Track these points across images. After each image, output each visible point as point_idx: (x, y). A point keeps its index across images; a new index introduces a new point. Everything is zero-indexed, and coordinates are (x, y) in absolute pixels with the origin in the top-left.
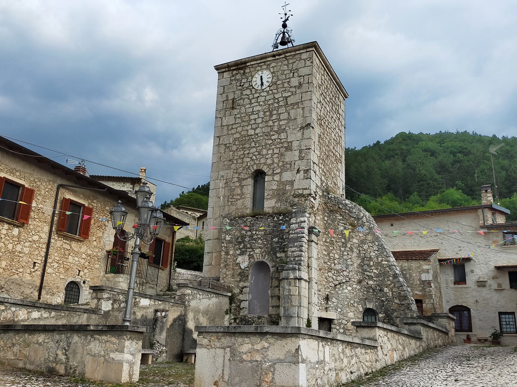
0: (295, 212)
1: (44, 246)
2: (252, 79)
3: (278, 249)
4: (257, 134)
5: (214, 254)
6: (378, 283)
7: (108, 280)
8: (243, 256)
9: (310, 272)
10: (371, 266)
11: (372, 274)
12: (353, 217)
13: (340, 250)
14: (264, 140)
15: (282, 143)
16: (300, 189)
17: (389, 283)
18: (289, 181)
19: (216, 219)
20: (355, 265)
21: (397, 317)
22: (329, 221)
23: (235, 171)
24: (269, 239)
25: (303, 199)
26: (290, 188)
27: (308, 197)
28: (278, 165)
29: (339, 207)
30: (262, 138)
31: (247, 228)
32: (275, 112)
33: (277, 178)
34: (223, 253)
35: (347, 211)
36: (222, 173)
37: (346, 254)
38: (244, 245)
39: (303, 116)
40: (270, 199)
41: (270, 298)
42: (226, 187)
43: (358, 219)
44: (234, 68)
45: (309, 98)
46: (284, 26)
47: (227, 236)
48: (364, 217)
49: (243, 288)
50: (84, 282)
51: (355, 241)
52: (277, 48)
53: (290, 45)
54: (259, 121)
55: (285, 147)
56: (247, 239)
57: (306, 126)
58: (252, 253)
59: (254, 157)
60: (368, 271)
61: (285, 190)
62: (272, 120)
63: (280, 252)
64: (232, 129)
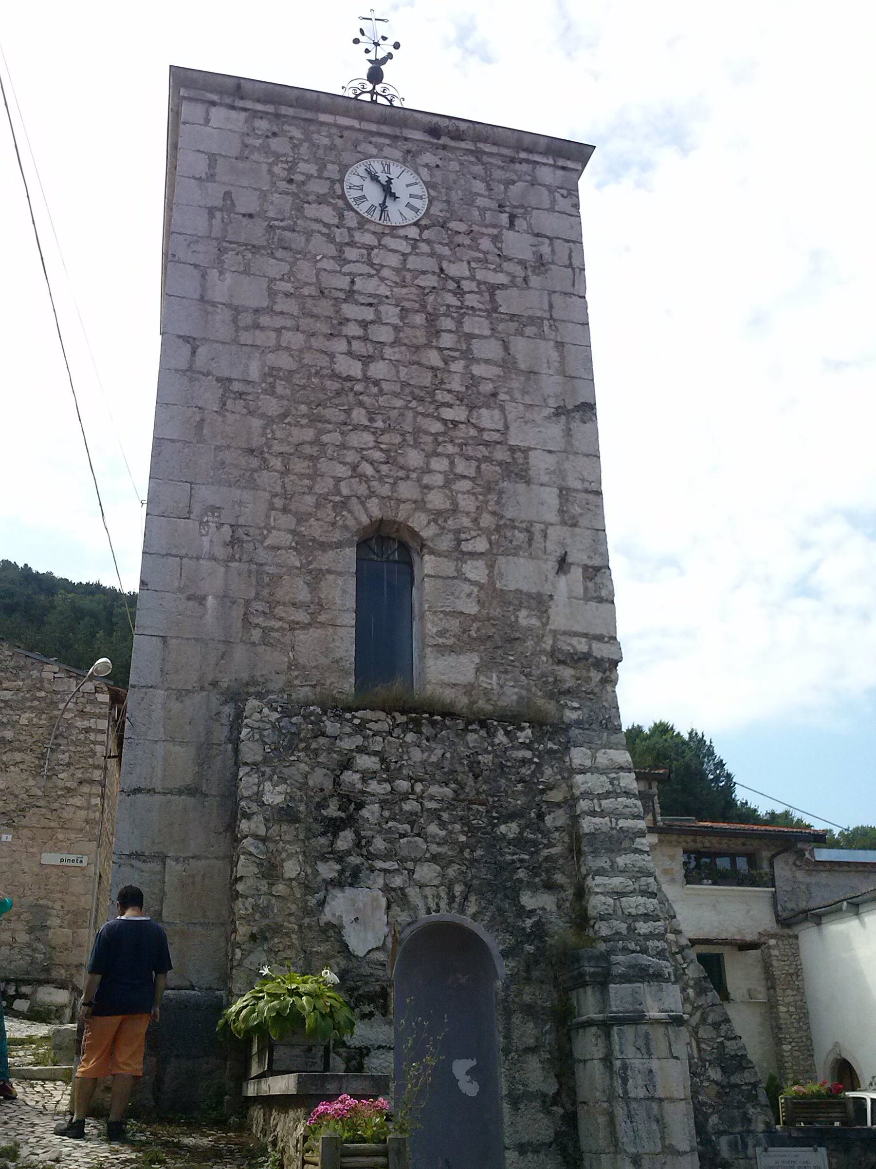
0: (579, 723)
3: (521, 874)
4: (376, 383)
18: (530, 596)
19: (181, 694)
21: (721, 1133)
23: (279, 503)
26: (534, 622)
28: (475, 521)
30: (399, 403)
32: (447, 323)
33: (476, 571)
34: (244, 867)
36: (207, 494)
39: (562, 372)
40: (452, 649)
41: (506, 1107)
42: (232, 558)
47: (268, 785)
55: (500, 464)
56: (371, 812)
58: (398, 881)
59: (368, 469)
62: (440, 349)
64: (257, 326)
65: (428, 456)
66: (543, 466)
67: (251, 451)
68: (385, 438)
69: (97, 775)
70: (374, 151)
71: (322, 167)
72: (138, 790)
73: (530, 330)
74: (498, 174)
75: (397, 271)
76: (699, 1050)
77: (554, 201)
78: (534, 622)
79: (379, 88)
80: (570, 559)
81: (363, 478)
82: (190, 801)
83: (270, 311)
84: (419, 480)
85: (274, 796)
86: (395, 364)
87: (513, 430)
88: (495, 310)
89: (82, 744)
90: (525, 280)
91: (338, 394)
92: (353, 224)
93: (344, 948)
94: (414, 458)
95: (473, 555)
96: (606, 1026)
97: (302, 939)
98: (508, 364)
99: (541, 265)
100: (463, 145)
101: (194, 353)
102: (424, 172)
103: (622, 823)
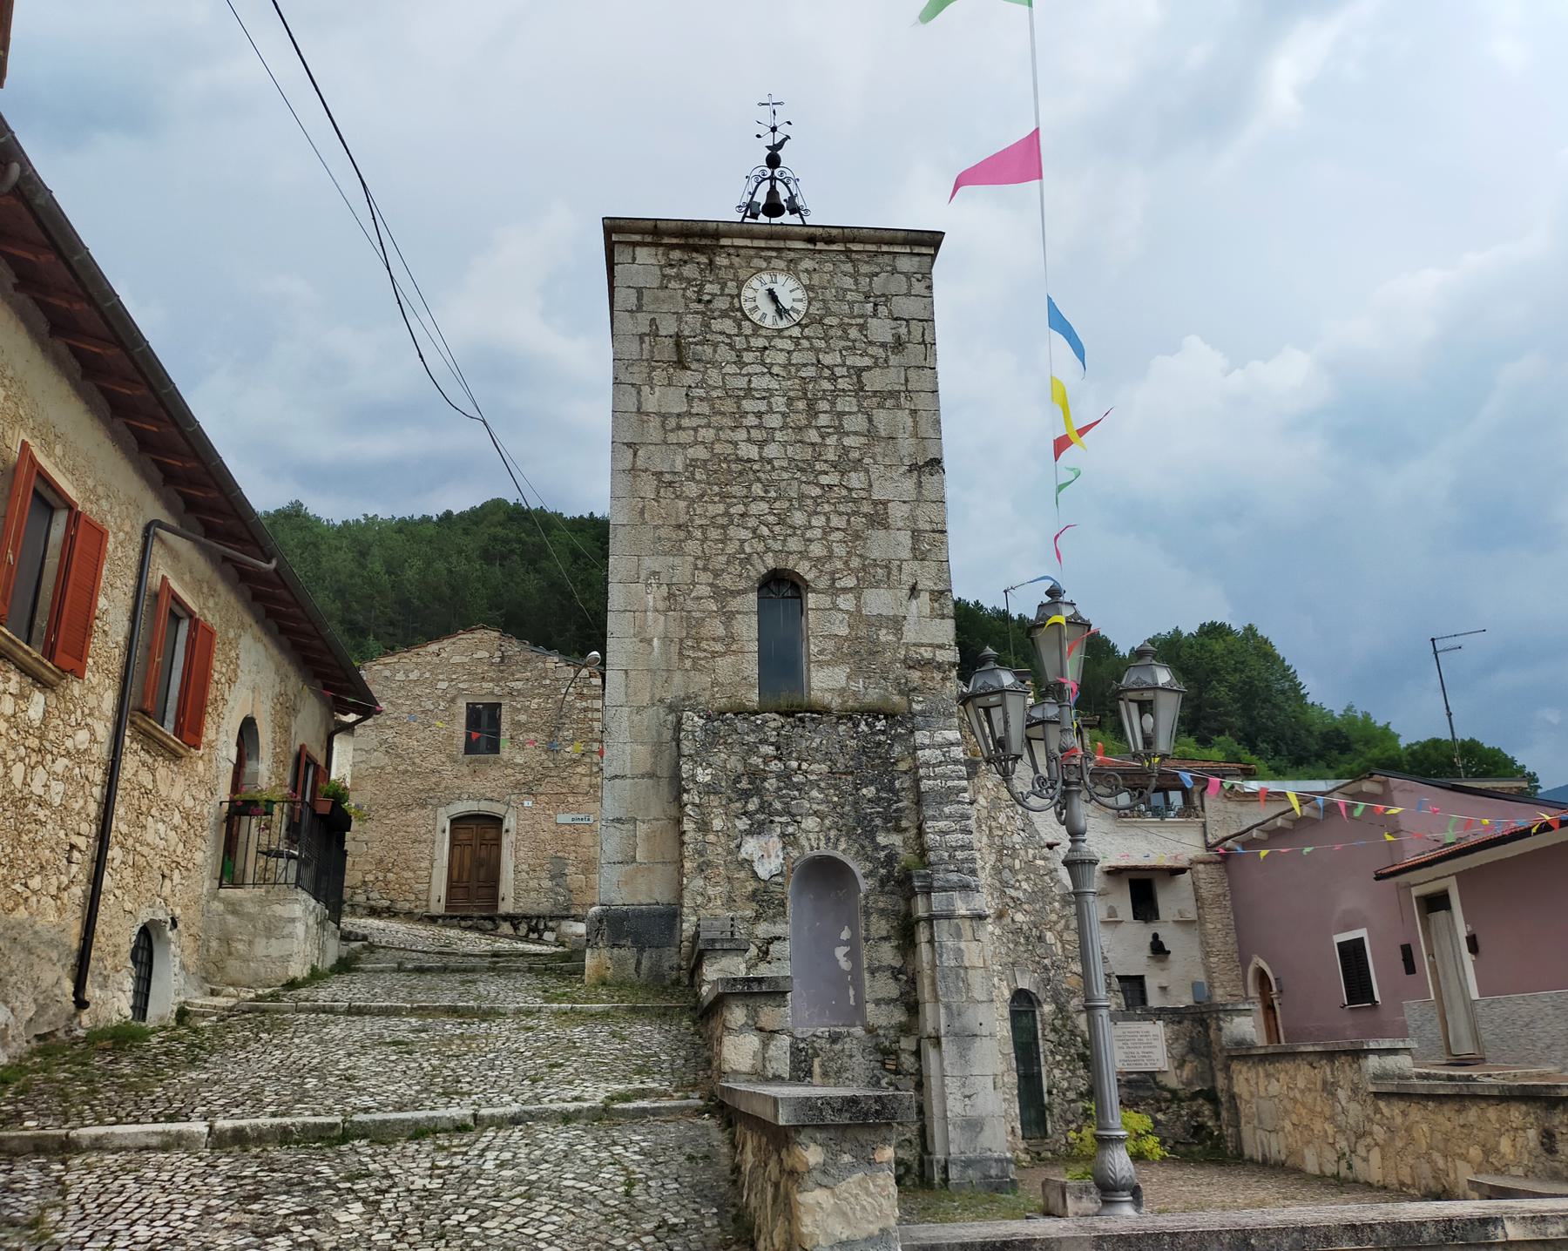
0: (922, 713)
1: (98, 775)
2: (739, 288)
4: (770, 461)
5: (642, 828)
7: (234, 912)
8: (762, 840)
14: (795, 483)
15: (855, 501)
16: (922, 645)
17: (1054, 917)
18: (887, 618)
19: (639, 710)
23: (700, 564)
25: (938, 676)
26: (891, 637)
28: (846, 563)
30: (785, 475)
31: (770, 750)
32: (823, 405)
34: (688, 826)
36: (651, 563)
38: (762, 802)
39: (915, 435)
40: (828, 663)
41: (867, 975)
42: (669, 609)
44: (674, 241)
45: (929, 387)
46: (773, 161)
49: (770, 941)
50: (174, 924)
52: (754, 216)
53: (787, 218)
54: (774, 421)
55: (865, 516)
57: (927, 464)
58: (790, 830)
59: (765, 531)
61: (876, 642)
62: (818, 428)
63: (888, 831)
64: (679, 427)
65: (810, 515)
66: (899, 514)
67: (679, 527)
68: (777, 505)
69: (596, 746)
70: (764, 265)
71: (724, 286)
72: (616, 777)
73: (889, 403)
74: (864, 269)
75: (784, 367)
76: (1064, 949)
77: (910, 286)
78: (891, 637)
79: (777, 172)
80: (920, 587)
81: (761, 538)
82: (650, 782)
83: (689, 414)
84: (803, 535)
85: (704, 776)
86: (784, 444)
87: (876, 485)
88: (862, 389)
89: (583, 721)
90: (886, 361)
91: (741, 473)
92: (749, 332)
93: (755, 875)
94: (798, 518)
95: (845, 590)
96: (930, 920)
97: (727, 869)
98: (871, 434)
99: (899, 345)
100: (834, 247)
101: (635, 455)
102: (804, 276)
103: (949, 783)
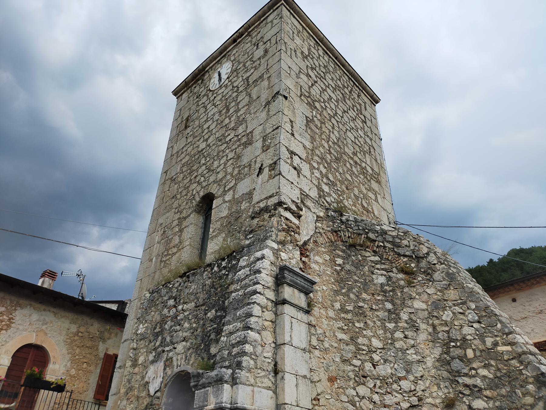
0: (249, 246)
6: (498, 404)
9: (280, 386)
10: (470, 361)
11: (478, 382)
12: (405, 256)
13: (385, 329)
20: (430, 361)
22: (348, 267)
24: (201, 315)
25: (266, 216)
27: (275, 209)
29: (368, 238)
35: (387, 245)
37: (401, 336)
43: (419, 259)
47: (141, 326)
48: (432, 255)
51: (418, 304)
60: (466, 375)
